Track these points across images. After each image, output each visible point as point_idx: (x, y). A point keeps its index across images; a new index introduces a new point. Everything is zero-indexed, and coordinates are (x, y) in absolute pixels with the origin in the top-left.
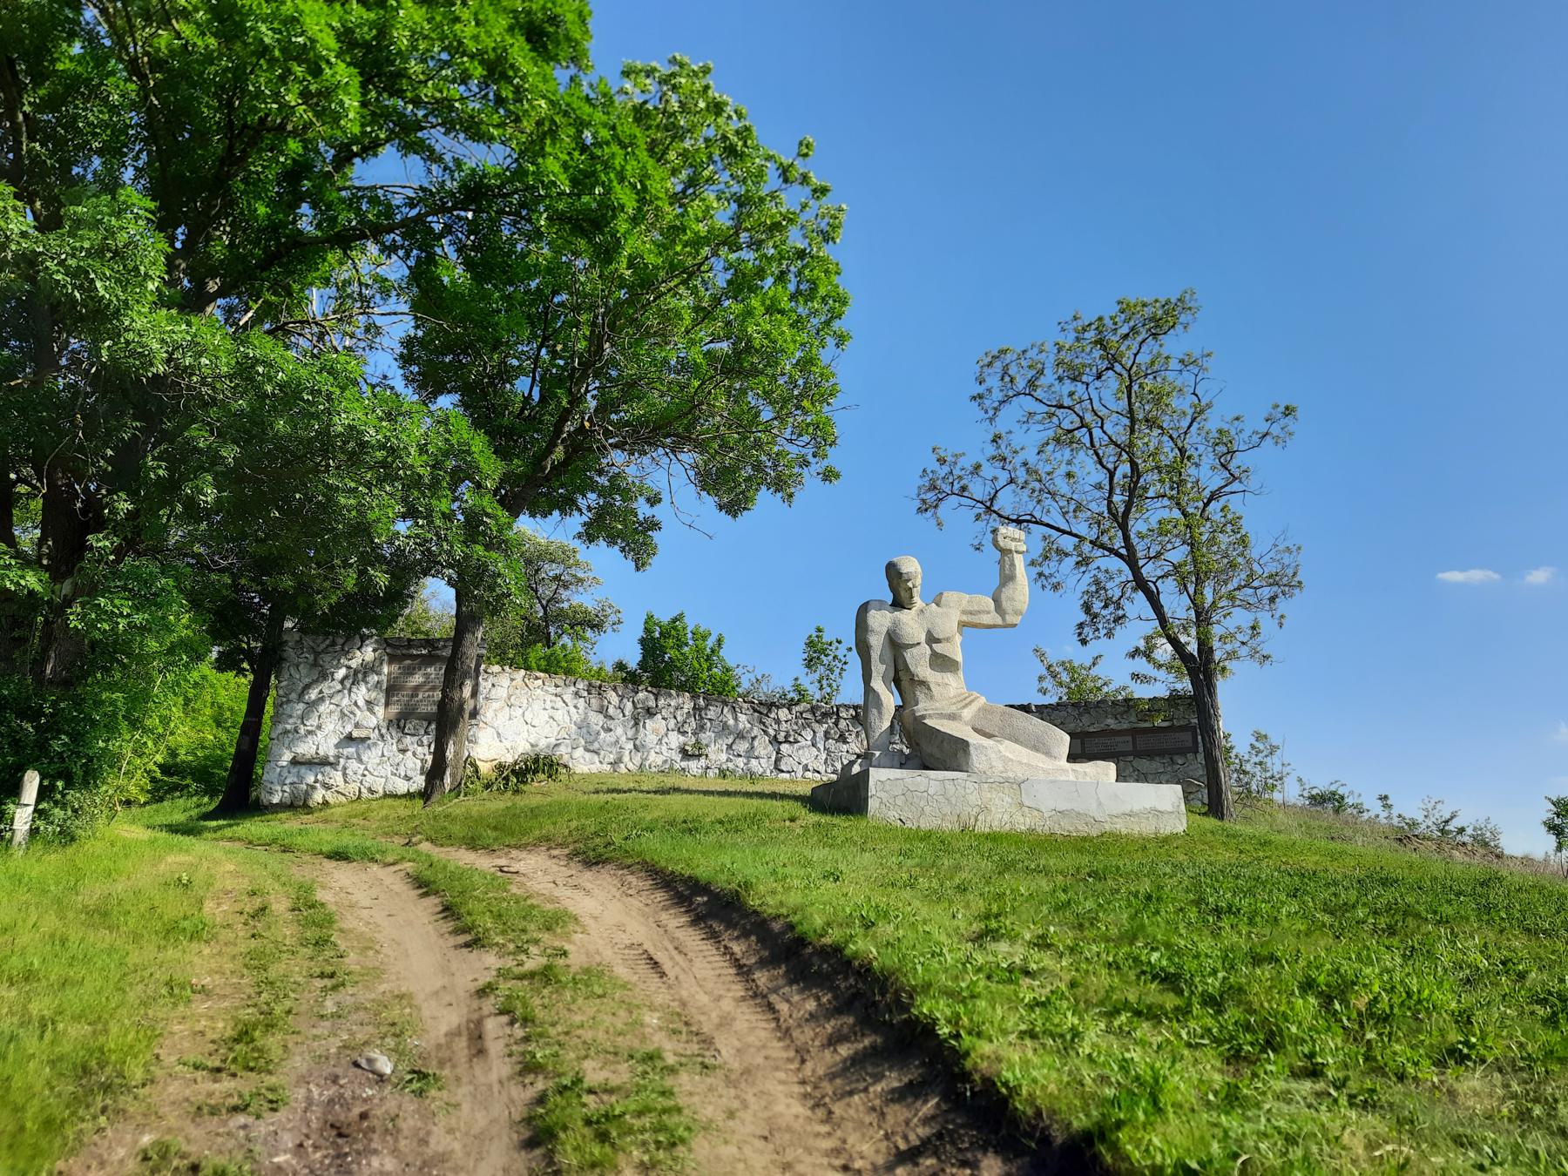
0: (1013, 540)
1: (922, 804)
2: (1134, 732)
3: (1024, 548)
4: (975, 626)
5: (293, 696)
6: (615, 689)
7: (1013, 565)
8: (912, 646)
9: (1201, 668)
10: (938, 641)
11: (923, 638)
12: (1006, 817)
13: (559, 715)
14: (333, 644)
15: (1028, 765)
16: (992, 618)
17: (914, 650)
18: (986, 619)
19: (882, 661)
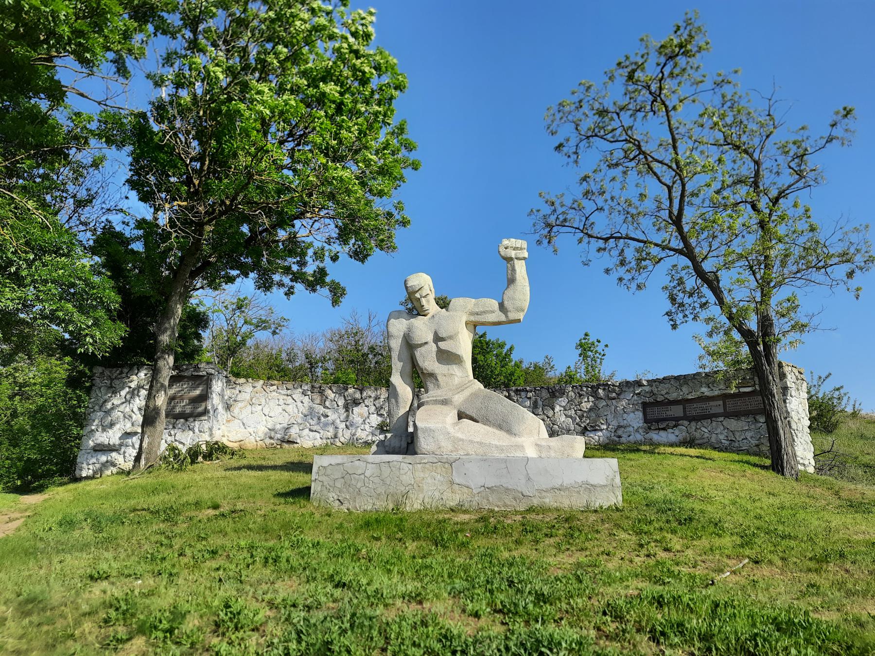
0: (515, 249)
2: (725, 397)
3: (526, 255)
5: (97, 408)
6: (330, 389)
7: (514, 270)
9: (761, 343)
10: (443, 339)
11: (430, 338)
12: (437, 494)
14: (122, 373)
15: (481, 443)
16: (499, 316)
17: (422, 350)
18: (491, 318)
19: (400, 360)
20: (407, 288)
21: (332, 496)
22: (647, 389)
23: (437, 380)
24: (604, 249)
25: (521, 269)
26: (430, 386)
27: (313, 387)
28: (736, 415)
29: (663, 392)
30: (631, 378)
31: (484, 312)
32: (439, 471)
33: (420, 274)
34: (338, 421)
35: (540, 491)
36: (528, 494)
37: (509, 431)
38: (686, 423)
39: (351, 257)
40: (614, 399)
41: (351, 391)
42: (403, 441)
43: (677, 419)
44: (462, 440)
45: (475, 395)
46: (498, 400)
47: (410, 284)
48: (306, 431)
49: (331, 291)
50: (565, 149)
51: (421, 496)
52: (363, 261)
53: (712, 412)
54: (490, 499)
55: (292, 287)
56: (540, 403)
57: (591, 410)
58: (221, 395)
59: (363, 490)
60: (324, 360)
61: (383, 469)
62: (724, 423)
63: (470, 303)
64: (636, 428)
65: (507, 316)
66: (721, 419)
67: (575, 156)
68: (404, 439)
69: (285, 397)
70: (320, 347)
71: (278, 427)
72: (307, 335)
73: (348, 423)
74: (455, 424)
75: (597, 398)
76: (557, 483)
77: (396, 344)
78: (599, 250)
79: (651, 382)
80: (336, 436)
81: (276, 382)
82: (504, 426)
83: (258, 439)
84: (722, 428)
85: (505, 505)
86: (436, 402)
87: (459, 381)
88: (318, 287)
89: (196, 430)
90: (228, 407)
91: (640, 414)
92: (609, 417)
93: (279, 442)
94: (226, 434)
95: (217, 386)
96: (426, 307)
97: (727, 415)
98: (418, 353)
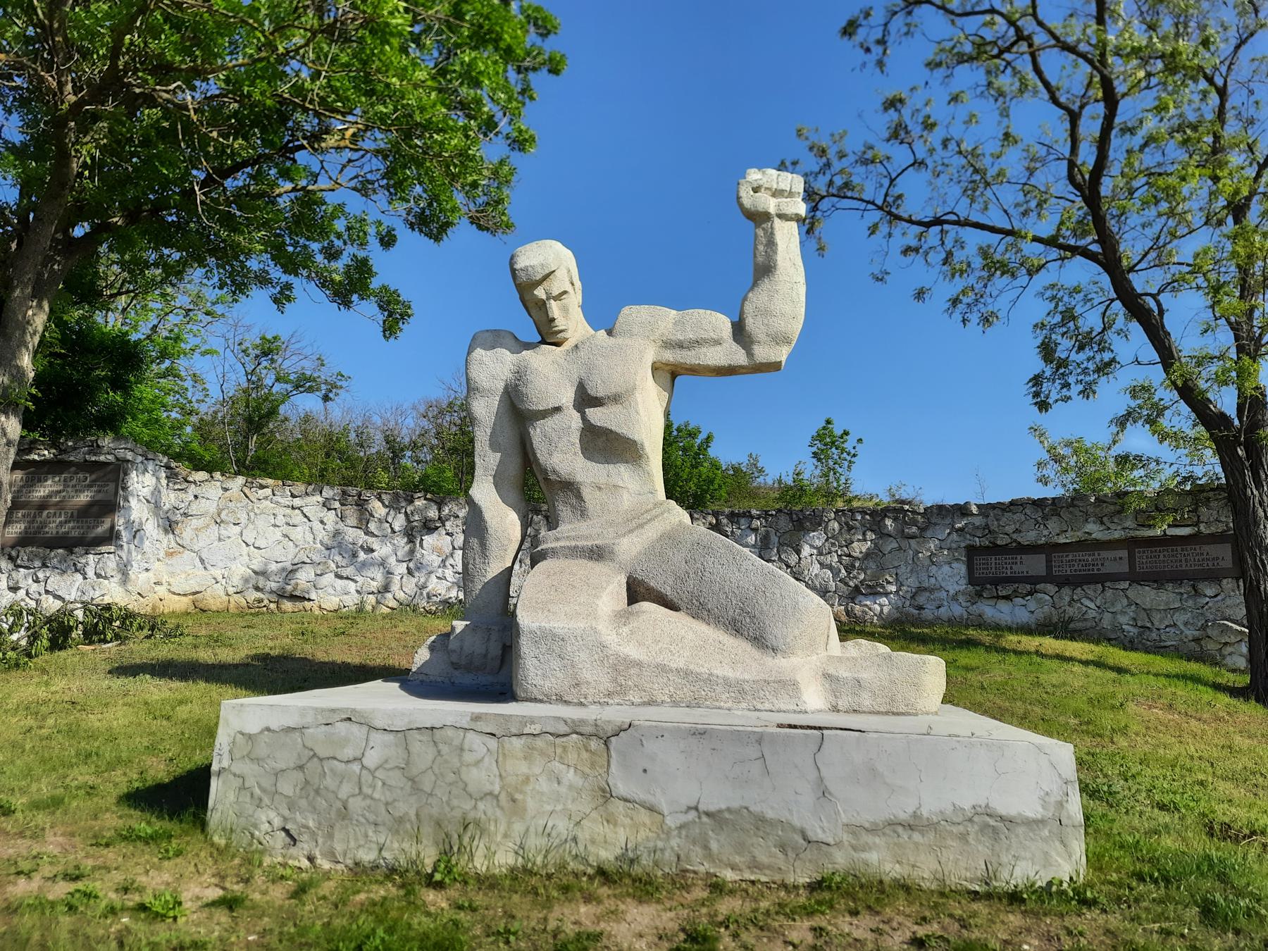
0: (777, 193)
1: (346, 790)
2: (1132, 544)
4: (694, 370)
6: (380, 499)
7: (771, 243)
8: (545, 414)
10: (597, 402)
11: (567, 397)
13: (297, 534)
15: (686, 674)
16: (729, 353)
17: (549, 423)
19: (494, 446)
20: (513, 271)
21: (267, 819)
22: (978, 521)
23: (579, 497)
24: (917, 250)
25: (788, 238)
26: (564, 511)
27: (344, 493)
28: (1157, 579)
29: (1010, 529)
30: (950, 501)
31: (698, 343)
32: (572, 757)
33: (548, 242)
34: (392, 560)
35: (854, 829)
36: (821, 836)
37: (760, 641)
38: (1051, 588)
39: (412, 226)
40: (913, 537)
41: (419, 503)
42: (482, 660)
43: (1034, 581)
44: (639, 664)
45: (671, 538)
46: (738, 563)
47: (521, 263)
48: (330, 577)
49: (381, 307)
50: (861, 34)
51: (518, 827)
52: (437, 239)
53: (1103, 571)
54: (714, 846)
55: (288, 286)
56: (774, 539)
57: (867, 555)
58: (155, 504)
59: (356, 804)
60: (414, 446)
61: (416, 747)
62: (1129, 593)
63: (666, 319)
64: (952, 592)
65: (750, 354)
66: (1125, 585)
67: (880, 49)
68: (494, 637)
69: (289, 511)
70: (409, 427)
71: (273, 567)
72: (388, 406)
73: (411, 565)
74: (621, 618)
75: (882, 534)
76: (902, 809)
77: (485, 410)
78: (907, 251)
79: (985, 509)
80: (386, 588)
81: (270, 481)
82: (747, 625)
83: (231, 591)
84: (1125, 602)
85: (755, 865)
86: (576, 552)
87: (632, 505)
88: (355, 297)
89: (90, 573)
90: (170, 526)
91: (961, 568)
92: (902, 570)
93: (274, 598)
94: (165, 578)
95: (142, 483)
96: (560, 323)
97: (1137, 578)
98: (538, 433)
